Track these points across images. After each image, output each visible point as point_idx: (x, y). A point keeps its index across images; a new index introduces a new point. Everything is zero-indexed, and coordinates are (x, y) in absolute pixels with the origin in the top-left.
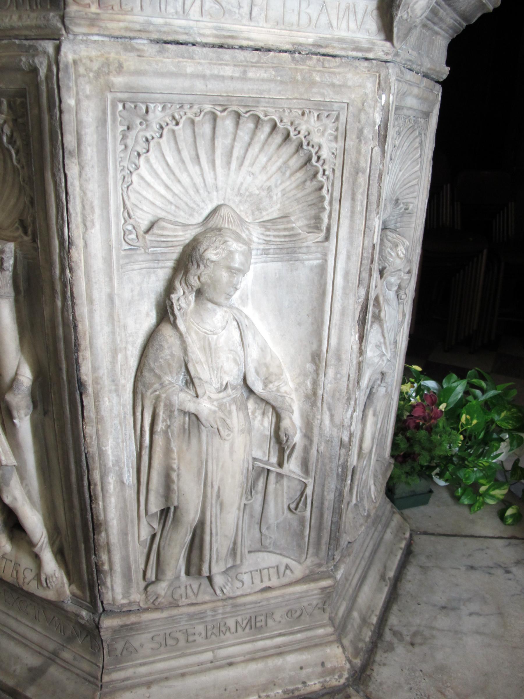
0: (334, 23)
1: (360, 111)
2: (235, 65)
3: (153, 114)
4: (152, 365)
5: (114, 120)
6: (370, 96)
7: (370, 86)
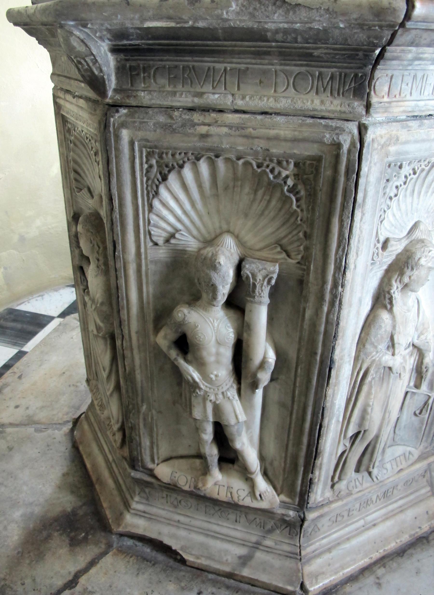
4: (373, 340)
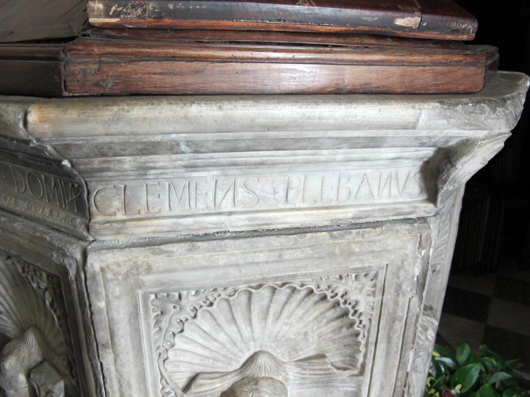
0: (375, 193)
1: (399, 269)
2: (270, 251)
3: (186, 300)
5: (146, 311)
6: (410, 256)
7: (411, 247)
